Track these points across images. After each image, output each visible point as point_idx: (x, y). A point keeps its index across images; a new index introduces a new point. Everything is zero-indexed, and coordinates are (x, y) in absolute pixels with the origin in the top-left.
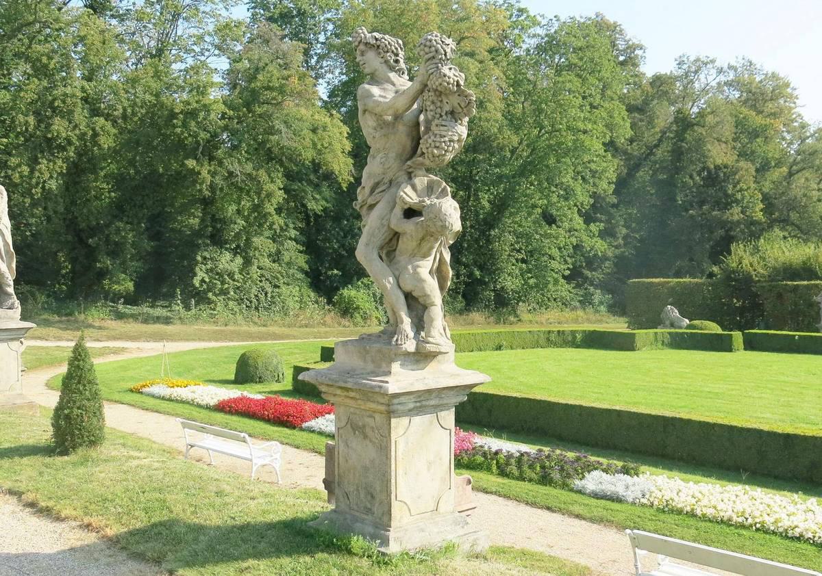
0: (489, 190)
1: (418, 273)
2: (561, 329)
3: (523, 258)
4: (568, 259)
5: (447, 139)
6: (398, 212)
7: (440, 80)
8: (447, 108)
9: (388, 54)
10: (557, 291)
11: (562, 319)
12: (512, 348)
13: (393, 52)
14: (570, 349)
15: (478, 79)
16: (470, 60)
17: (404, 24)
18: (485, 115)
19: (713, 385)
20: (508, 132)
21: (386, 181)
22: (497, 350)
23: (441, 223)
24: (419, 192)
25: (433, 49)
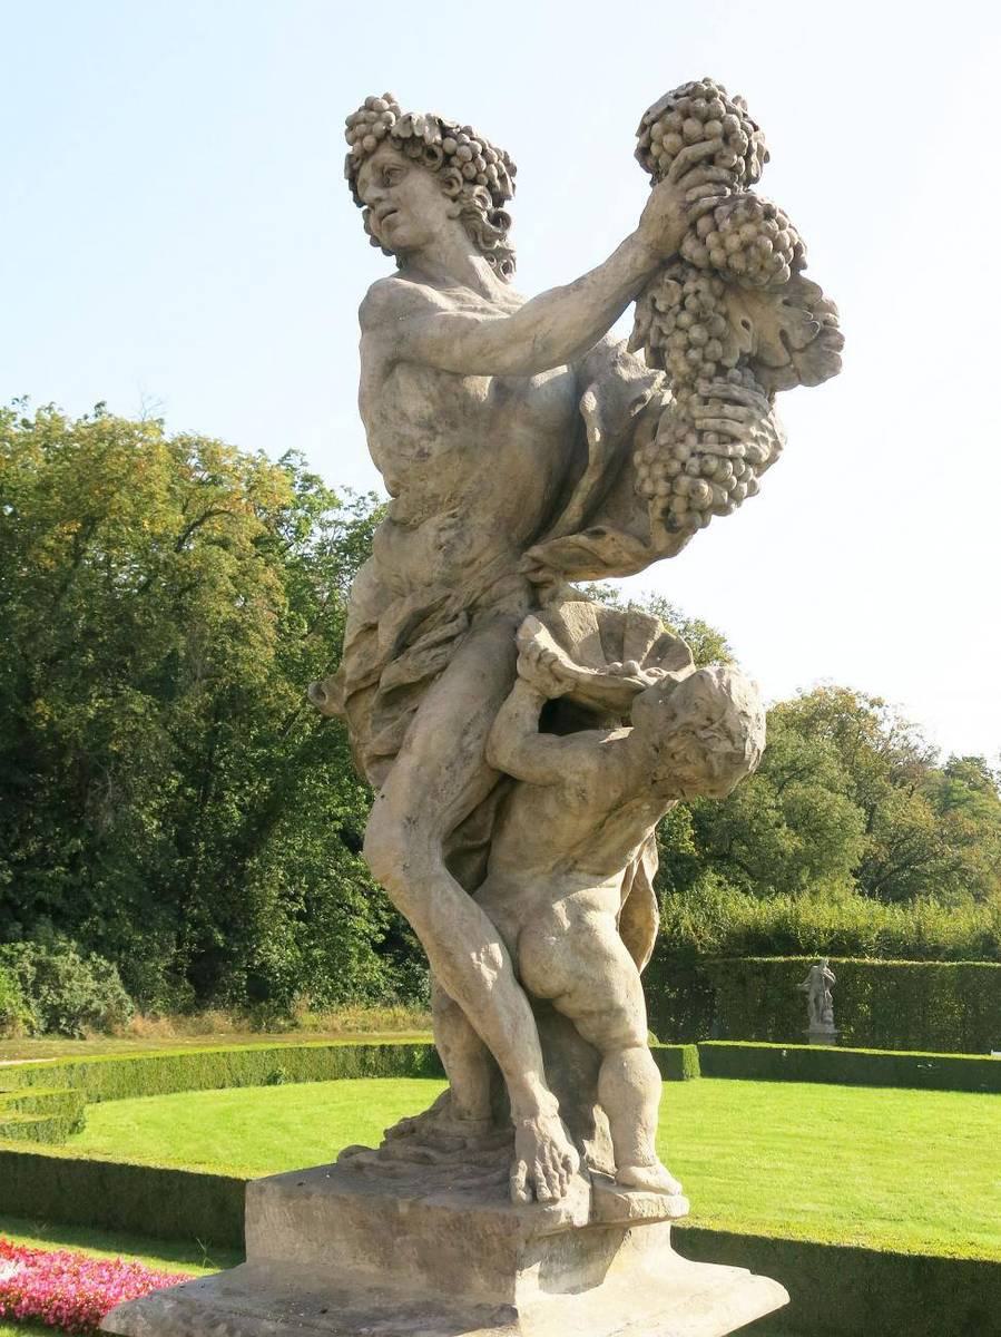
0: (242, 787)
1: (589, 930)
2: (388, 1043)
3: (301, 911)
4: (382, 913)
5: (742, 449)
6: (523, 705)
7: (749, 230)
8: (745, 343)
9: (478, 189)
10: (365, 970)
11: (370, 1023)
12: (297, 1080)
13: (490, 186)
14: (405, 1081)
15: (235, 586)
16: (222, 551)
17: (104, 476)
18: (244, 651)
19: (684, 1147)
20: (284, 686)
21: (454, 607)
22: (269, 1083)
23: (726, 746)
24: (576, 649)
25: (717, 126)
